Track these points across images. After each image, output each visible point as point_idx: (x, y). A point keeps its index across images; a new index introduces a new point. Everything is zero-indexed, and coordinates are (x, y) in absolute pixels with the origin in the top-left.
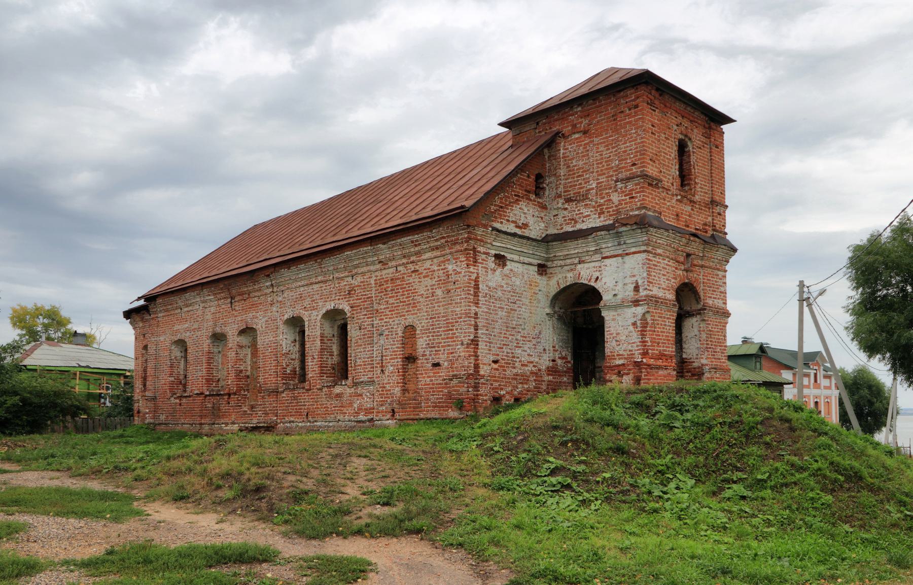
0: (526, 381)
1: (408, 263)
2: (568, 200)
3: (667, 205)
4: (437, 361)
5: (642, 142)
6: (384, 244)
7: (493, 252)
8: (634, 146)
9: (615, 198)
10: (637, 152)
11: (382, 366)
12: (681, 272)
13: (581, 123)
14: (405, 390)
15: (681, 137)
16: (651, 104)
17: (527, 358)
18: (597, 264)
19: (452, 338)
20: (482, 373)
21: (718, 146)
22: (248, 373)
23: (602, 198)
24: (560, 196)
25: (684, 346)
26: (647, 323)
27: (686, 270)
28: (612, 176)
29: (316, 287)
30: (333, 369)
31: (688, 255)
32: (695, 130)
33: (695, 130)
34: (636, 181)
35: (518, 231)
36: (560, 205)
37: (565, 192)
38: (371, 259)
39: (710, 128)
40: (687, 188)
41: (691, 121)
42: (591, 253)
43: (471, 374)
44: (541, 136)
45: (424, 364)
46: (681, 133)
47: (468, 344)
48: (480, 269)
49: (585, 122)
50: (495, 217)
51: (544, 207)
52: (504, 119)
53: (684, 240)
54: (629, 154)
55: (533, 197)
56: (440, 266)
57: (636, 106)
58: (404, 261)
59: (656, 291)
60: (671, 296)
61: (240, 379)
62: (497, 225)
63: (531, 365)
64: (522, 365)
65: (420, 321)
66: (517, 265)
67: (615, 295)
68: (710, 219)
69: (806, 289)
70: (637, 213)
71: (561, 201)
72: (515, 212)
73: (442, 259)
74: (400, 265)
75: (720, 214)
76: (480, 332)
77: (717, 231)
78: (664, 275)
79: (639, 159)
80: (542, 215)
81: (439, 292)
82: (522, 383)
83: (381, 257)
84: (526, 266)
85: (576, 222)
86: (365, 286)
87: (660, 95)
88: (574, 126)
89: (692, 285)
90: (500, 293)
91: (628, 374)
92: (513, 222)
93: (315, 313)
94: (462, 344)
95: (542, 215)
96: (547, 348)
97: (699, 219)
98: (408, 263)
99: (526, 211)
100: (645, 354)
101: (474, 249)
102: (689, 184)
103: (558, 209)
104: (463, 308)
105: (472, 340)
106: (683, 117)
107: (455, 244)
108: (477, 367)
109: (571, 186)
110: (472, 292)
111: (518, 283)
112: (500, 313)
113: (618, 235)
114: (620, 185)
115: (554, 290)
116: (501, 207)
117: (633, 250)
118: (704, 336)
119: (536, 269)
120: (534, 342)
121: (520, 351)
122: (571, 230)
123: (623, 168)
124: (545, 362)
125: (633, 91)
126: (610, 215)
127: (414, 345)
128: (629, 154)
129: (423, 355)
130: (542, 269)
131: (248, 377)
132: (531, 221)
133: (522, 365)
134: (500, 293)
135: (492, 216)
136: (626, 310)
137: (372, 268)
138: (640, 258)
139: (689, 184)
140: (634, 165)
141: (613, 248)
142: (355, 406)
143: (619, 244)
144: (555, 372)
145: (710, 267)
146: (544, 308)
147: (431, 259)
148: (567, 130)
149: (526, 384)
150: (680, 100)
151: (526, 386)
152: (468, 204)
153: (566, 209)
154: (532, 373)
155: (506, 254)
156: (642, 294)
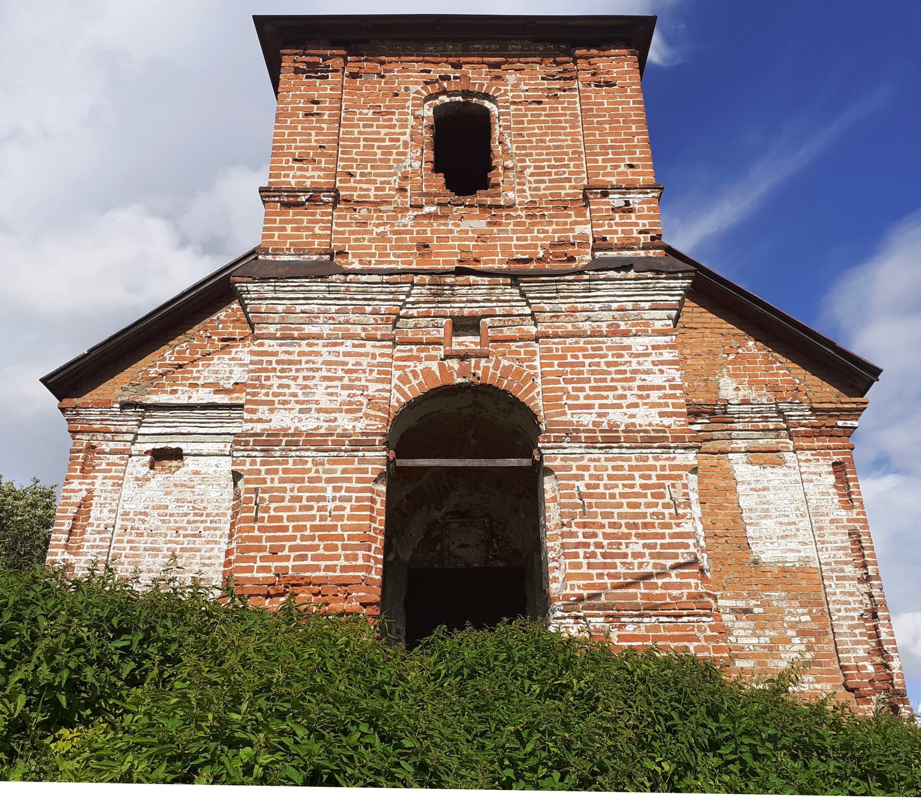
32: (511, 78)
48: (98, 482)
50: (163, 385)
90: (154, 521)
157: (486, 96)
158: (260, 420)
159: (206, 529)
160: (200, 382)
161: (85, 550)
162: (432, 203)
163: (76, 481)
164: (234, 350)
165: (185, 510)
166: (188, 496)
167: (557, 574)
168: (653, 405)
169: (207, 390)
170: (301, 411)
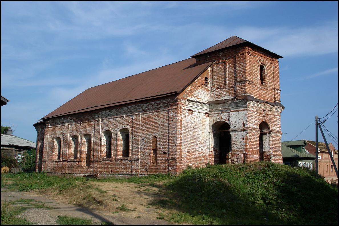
7: (188, 109)
15: (261, 64)
20: (183, 157)
25: (263, 146)
26: (248, 138)
42: (226, 109)
43: (179, 157)
48: (183, 115)
50: (189, 95)
55: (204, 86)
60: (257, 127)
63: (202, 153)
64: (199, 153)
68: (273, 96)
72: (197, 93)
76: (182, 140)
78: (254, 119)
79: (244, 74)
85: (221, 97)
92: (196, 96)
109: (218, 83)
116: (191, 91)
121: (198, 148)
134: (190, 124)
139: (264, 83)
140: (243, 76)
149: (200, 161)
155: (193, 109)
157: (265, 65)
158: (249, 125)
161: (182, 130)
164: (199, 89)
165: (194, 123)
167: (271, 151)
168: (279, 127)
170: (252, 124)
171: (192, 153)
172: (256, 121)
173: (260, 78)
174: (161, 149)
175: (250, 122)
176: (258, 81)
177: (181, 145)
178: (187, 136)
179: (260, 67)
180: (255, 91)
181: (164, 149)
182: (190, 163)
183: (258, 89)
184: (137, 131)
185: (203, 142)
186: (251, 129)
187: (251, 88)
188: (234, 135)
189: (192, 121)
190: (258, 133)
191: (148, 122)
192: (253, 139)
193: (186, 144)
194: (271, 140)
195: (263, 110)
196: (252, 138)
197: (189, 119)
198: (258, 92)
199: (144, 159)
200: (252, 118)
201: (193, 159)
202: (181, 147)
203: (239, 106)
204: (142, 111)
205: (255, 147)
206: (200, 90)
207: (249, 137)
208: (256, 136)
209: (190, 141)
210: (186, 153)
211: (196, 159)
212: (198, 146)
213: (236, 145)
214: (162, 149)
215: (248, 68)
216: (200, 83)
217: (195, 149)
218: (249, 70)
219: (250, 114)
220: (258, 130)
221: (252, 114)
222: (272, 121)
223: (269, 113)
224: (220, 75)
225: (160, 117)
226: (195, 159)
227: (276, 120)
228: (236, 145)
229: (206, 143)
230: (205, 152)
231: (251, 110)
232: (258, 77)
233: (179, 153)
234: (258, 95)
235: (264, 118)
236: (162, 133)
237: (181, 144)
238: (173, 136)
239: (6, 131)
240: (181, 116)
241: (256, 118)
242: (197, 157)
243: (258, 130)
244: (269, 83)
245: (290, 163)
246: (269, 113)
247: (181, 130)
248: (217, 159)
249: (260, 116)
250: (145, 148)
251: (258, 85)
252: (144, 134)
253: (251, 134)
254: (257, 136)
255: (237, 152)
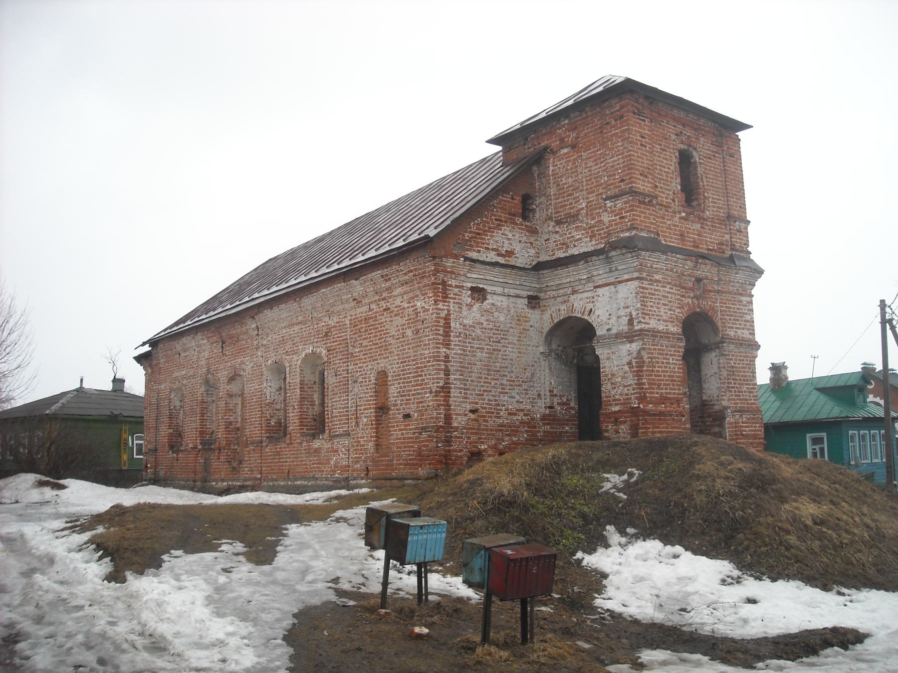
0: (516, 432)
1: (379, 300)
2: (559, 223)
3: (672, 225)
4: (408, 411)
5: (630, 155)
6: (356, 279)
7: (469, 285)
8: (621, 160)
9: (606, 218)
10: (624, 167)
11: (357, 418)
12: (690, 300)
13: (569, 136)
14: (378, 446)
15: (682, 146)
16: (639, 113)
17: (517, 406)
18: (589, 294)
19: (421, 385)
20: (455, 424)
21: (734, 156)
22: (238, 425)
23: (593, 219)
24: (550, 218)
25: (704, 386)
26: (644, 362)
27: (696, 297)
28: (602, 194)
29: (296, 328)
30: (315, 420)
31: (699, 280)
32: (702, 139)
33: (702, 139)
34: (625, 198)
35: (501, 260)
36: (551, 228)
37: (556, 213)
38: (345, 297)
39: (721, 135)
40: (695, 203)
41: (695, 130)
42: (583, 282)
43: (441, 427)
44: (528, 149)
45: (396, 414)
46: (682, 143)
47: (436, 392)
48: (451, 305)
49: (573, 135)
50: (471, 246)
51: (533, 231)
52: (492, 135)
53: (689, 263)
54: (617, 169)
55: (519, 220)
56: (409, 303)
57: (622, 117)
58: (377, 298)
59: (653, 324)
60: (675, 329)
61: (229, 432)
62: (473, 255)
63: (521, 414)
64: (510, 414)
65: (392, 366)
66: (500, 298)
67: (608, 330)
68: (727, 237)
69: (888, 310)
70: (627, 234)
71: (552, 223)
72: (497, 239)
73: (411, 295)
74: (372, 302)
75: (739, 231)
76: (452, 377)
77: (737, 250)
78: (664, 305)
79: (628, 174)
80: (532, 240)
81: (409, 332)
82: (509, 435)
83: (355, 294)
84: (512, 299)
85: (568, 247)
86: (341, 326)
87: (651, 103)
88: (562, 140)
89: (706, 314)
91: (625, 422)
92: (493, 250)
93: (295, 357)
94: (431, 392)
95: (532, 240)
96: (542, 393)
97: (711, 239)
98: (379, 300)
99: (510, 236)
100: (642, 399)
101: (444, 283)
102: (697, 199)
103: (549, 232)
104: (431, 351)
105: (442, 387)
106: (684, 125)
107: (423, 277)
108: (448, 418)
109: (561, 207)
110: (441, 332)
111: (502, 319)
112: (479, 354)
113: (609, 260)
114: (609, 204)
115: (547, 327)
116: (479, 234)
117: (626, 277)
118: (725, 373)
119: (526, 301)
120: (525, 386)
122: (563, 255)
123: (613, 184)
124: (540, 408)
125: (617, 100)
126: (602, 238)
127: (386, 393)
128: (617, 169)
129: (396, 405)
130: (534, 301)
131: (238, 429)
132: (517, 247)
133: (510, 414)
134: (479, 331)
135: (467, 244)
136: (620, 347)
137: (347, 306)
138: (633, 286)
139: (697, 199)
140: (622, 181)
141: (605, 275)
142: (332, 463)
143: (611, 271)
144: (554, 420)
145: (730, 293)
146: (536, 345)
147: (402, 295)
148: (555, 144)
149: (515, 435)
150: (678, 108)
151: (515, 439)
152: (432, 233)
153: (557, 232)
154: (522, 422)
155: (485, 287)
156: (636, 328)
157: (695, 149)
158: (646, 323)
159: (502, 338)
160: (490, 247)
162: (684, 211)
163: (441, 303)
166: (491, 318)
169: (494, 253)
170: (659, 320)
171: (488, 413)
172: (670, 310)
173: (679, 187)
174: (397, 405)
175: (648, 315)
176: (674, 194)
177: (449, 392)
178: (469, 364)
179: (677, 154)
180: (665, 223)
181: (406, 404)
182: (483, 443)
183: (676, 219)
184: (341, 359)
185: (523, 382)
186: (652, 336)
187: (651, 214)
188: (606, 356)
189: (483, 320)
190: (679, 347)
191: (366, 331)
192: (663, 363)
193: (465, 389)
194: (724, 367)
195: (693, 279)
196: (658, 362)
197: (473, 314)
198: (674, 225)
199: (360, 435)
200: (658, 303)
201: (491, 430)
202: (449, 397)
203: (616, 270)
204: (351, 300)
205: (671, 389)
206: (506, 232)
207: (648, 358)
208: (671, 355)
209: (481, 378)
210: (466, 415)
211: (501, 430)
212: (507, 393)
213: (612, 384)
214: (401, 405)
215: (638, 157)
216: (505, 209)
217: (496, 400)
218: (643, 163)
219: (650, 291)
220: (678, 339)
221: (655, 290)
222: (725, 311)
223: (716, 287)
224: (565, 184)
225: (393, 314)
226: (496, 430)
227: (738, 309)
228: (612, 384)
229: (531, 384)
230: (529, 410)
231: (651, 280)
232: (674, 184)
233: (442, 416)
234: (675, 234)
235: (699, 304)
236: (399, 359)
237: (450, 388)
238: (426, 367)
239: (118, 382)
240: (445, 308)
241: (670, 302)
242: (502, 426)
243: (678, 339)
244: (710, 199)
245: (824, 435)
246: (716, 287)
247: (448, 349)
248: (571, 428)
249: (682, 296)
250: (360, 406)
251: (675, 206)
252: (356, 364)
253: (655, 349)
254: (675, 355)
255: (616, 405)
